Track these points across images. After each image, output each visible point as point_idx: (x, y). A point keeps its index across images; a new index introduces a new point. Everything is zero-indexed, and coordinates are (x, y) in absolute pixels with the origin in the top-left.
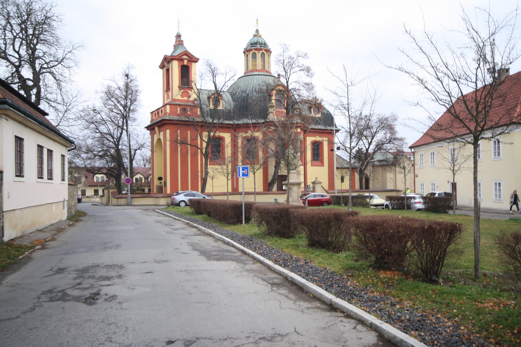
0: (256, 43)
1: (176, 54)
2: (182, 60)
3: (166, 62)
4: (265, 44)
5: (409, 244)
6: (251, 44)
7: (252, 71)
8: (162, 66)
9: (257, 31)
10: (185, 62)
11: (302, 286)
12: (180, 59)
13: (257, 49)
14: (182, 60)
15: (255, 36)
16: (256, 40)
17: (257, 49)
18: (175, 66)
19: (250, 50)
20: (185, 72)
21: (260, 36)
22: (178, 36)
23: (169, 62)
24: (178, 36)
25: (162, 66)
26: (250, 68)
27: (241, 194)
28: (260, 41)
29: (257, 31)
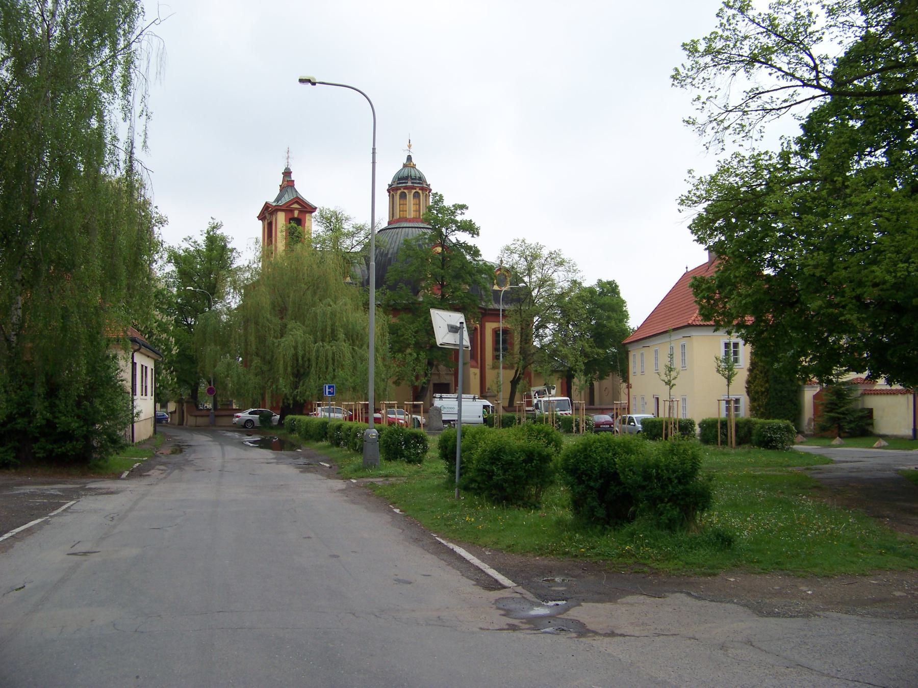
0: (406, 178)
1: (282, 202)
2: (292, 211)
4: (420, 178)
6: (399, 179)
9: (409, 158)
12: (287, 209)
13: (408, 184)
15: (405, 166)
17: (408, 184)
18: (281, 218)
19: (397, 189)
21: (414, 166)
22: (287, 173)
24: (287, 173)
25: (262, 217)
26: (397, 216)
29: (409, 158)
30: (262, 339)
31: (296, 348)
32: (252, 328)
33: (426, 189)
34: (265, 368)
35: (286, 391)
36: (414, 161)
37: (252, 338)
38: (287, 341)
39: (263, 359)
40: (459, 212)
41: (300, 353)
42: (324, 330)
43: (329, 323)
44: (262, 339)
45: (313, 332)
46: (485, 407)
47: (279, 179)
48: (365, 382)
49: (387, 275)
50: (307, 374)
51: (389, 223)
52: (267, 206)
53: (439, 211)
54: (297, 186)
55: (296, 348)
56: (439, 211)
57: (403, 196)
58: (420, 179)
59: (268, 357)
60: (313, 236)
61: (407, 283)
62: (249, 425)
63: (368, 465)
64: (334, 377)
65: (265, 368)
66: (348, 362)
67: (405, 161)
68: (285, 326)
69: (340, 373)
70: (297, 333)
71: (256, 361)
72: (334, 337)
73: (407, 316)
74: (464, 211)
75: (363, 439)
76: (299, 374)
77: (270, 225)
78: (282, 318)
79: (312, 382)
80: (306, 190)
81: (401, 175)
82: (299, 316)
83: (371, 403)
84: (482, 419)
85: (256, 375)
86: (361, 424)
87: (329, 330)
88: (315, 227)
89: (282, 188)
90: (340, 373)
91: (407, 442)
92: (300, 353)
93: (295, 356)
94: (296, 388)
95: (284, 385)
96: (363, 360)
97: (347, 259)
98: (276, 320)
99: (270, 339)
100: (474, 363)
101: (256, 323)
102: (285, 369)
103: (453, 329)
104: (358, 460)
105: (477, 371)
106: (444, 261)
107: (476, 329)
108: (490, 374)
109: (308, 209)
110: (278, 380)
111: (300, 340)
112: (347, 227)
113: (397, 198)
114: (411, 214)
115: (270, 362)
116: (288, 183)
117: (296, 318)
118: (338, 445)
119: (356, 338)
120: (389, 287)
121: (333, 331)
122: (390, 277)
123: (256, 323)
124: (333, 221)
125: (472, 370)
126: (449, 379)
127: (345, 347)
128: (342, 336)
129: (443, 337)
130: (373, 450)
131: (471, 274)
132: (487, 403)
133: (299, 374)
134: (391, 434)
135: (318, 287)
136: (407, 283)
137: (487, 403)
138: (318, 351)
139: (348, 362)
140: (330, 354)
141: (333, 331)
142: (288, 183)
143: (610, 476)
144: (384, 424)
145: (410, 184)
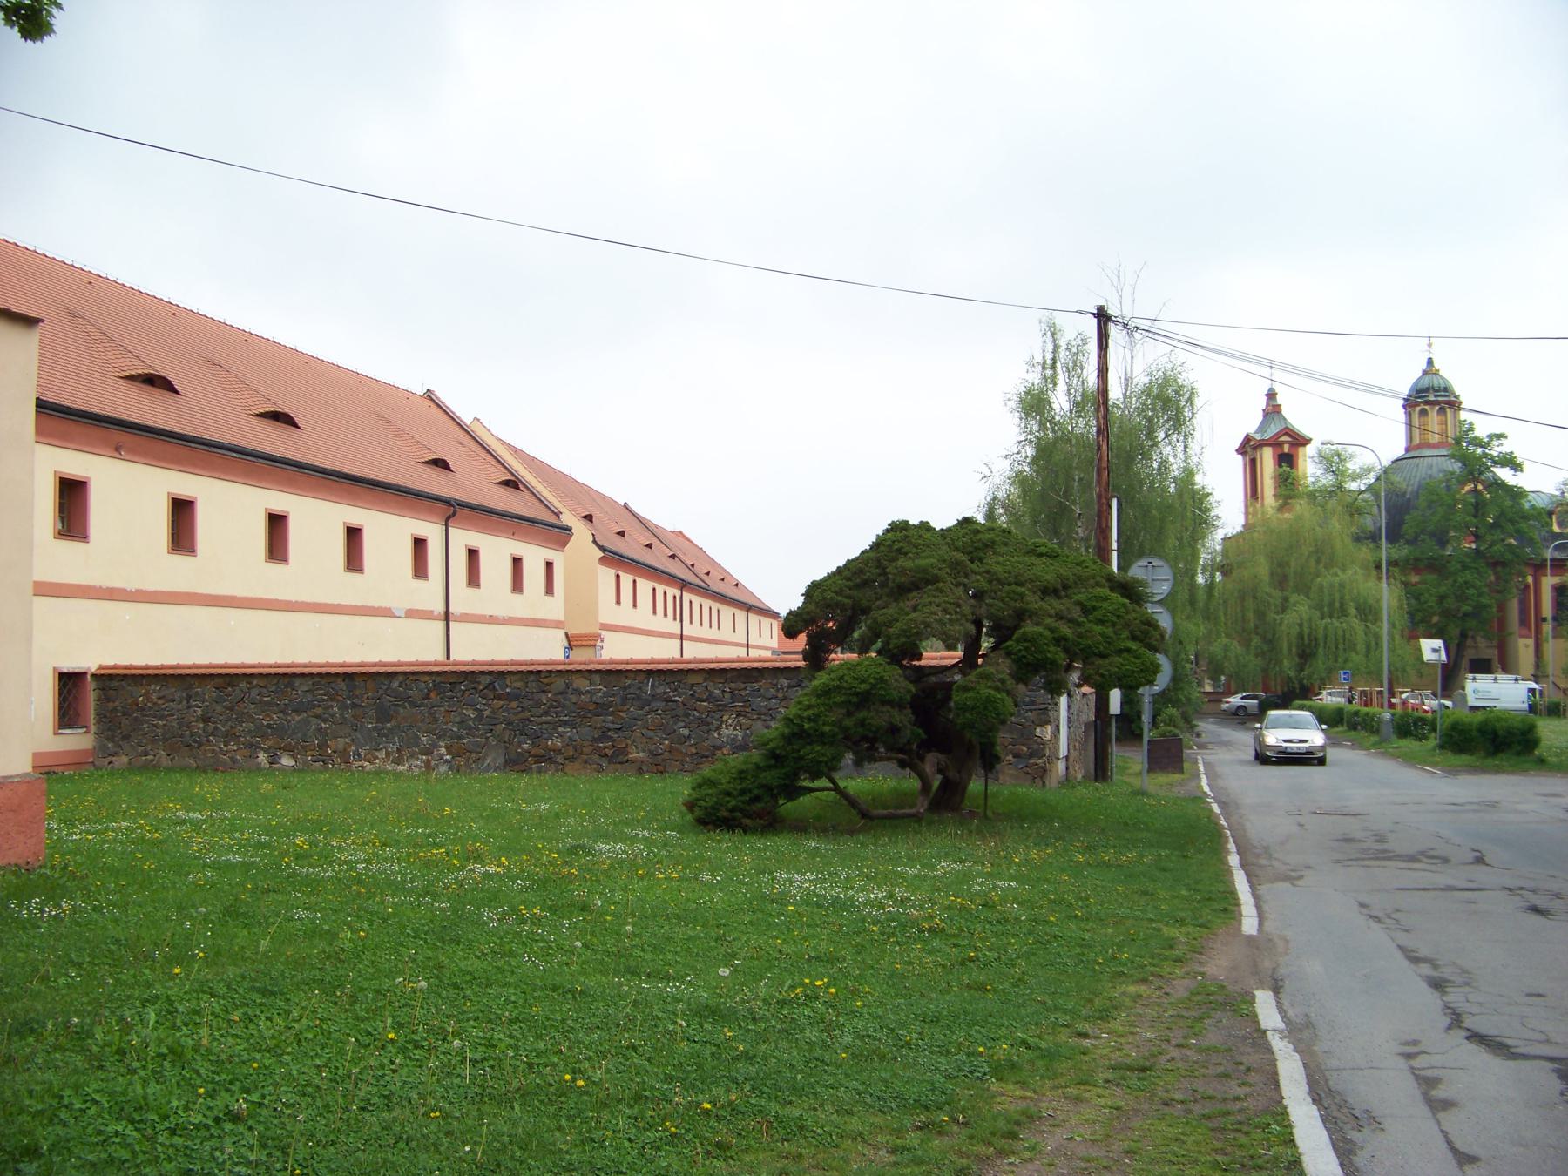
0: (1427, 390)
1: (1267, 436)
2: (1280, 445)
3: (1248, 448)
4: (1446, 389)
5: (1512, 541)
6: (1418, 392)
7: (1419, 447)
8: (1242, 450)
9: (1430, 362)
10: (1286, 448)
11: (1465, 758)
12: (1274, 443)
13: (1430, 399)
14: (1280, 445)
15: (1425, 373)
16: (1426, 382)
17: (1430, 399)
18: (1267, 457)
19: (1417, 404)
20: (1287, 460)
21: (1436, 373)
22: (1271, 395)
23: (1255, 448)
24: (1271, 395)
25: (1242, 450)
26: (1417, 441)
27: (1551, 1059)
28: (1436, 384)
29: (1430, 362)
30: (1261, 615)
31: (1301, 625)
32: (1250, 603)
33: (1455, 405)
34: (1265, 648)
35: (1291, 673)
36: (1437, 365)
37: (1250, 615)
38: (1290, 618)
39: (1264, 638)
40: (1495, 443)
41: (1306, 631)
42: (1331, 604)
43: (1337, 596)
44: (1261, 615)
45: (1319, 607)
46: (1532, 691)
47: (1262, 403)
48: (1380, 669)
49: (1405, 527)
50: (1313, 655)
51: (1407, 450)
52: (1248, 439)
53: (1469, 443)
54: (1285, 412)
55: (1301, 625)
56: (1469, 443)
57: (1423, 413)
58: (1447, 390)
59: (1269, 636)
60: (1310, 480)
61: (1432, 535)
62: (1241, 712)
63: (1385, 740)
64: (1346, 661)
65: (1265, 648)
66: (1361, 647)
67: (1424, 366)
68: (1286, 599)
69: (1354, 656)
70: (1301, 610)
71: (1256, 641)
72: (1343, 612)
73: (1431, 577)
74: (1502, 441)
75: (1380, 721)
76: (1305, 654)
77: (1253, 462)
78: (1282, 590)
79: (1320, 664)
80: (1297, 416)
81: (1420, 386)
82: (1304, 589)
83: (1385, 689)
84: (1526, 706)
85: (1257, 656)
86: (1377, 710)
87: (1337, 605)
88: (1310, 470)
89: (1266, 414)
90: (1354, 656)
91: (1415, 724)
92: (1306, 631)
93: (1301, 636)
94: (1302, 670)
95: (1288, 666)
96: (1377, 637)
97: (1353, 508)
98: (1277, 593)
99: (1271, 616)
100: (1525, 631)
101: (1255, 597)
102: (1290, 650)
103: (1435, 651)
104: (1374, 738)
105: (1531, 642)
106: (1478, 507)
107: (1527, 586)
108: (1550, 647)
109: (1300, 441)
110: (1281, 662)
111: (1305, 617)
112: (1353, 466)
113: (1416, 416)
114: (1436, 439)
115: (1271, 642)
116: (1273, 410)
117: (1298, 590)
118: (1355, 729)
119: (1368, 612)
120: (1408, 542)
121: (1342, 604)
122: (1409, 529)
123: (1255, 597)
124: (1333, 461)
125: (1522, 642)
126: (1493, 654)
127: (1355, 622)
128: (1352, 611)
129: (1428, 656)
130: (1387, 730)
131: (1512, 521)
132: (1534, 685)
133: (1305, 654)
134: (1402, 717)
135: (1323, 554)
136: (1432, 535)
137: (1534, 685)
138: (1326, 628)
139: (1361, 647)
140: (1340, 633)
141: (1342, 604)
142: (1273, 410)
143: (1495, 733)
144: (1399, 710)
145: (1432, 398)
